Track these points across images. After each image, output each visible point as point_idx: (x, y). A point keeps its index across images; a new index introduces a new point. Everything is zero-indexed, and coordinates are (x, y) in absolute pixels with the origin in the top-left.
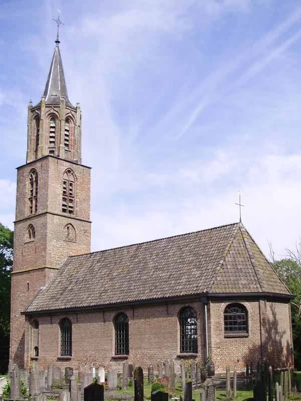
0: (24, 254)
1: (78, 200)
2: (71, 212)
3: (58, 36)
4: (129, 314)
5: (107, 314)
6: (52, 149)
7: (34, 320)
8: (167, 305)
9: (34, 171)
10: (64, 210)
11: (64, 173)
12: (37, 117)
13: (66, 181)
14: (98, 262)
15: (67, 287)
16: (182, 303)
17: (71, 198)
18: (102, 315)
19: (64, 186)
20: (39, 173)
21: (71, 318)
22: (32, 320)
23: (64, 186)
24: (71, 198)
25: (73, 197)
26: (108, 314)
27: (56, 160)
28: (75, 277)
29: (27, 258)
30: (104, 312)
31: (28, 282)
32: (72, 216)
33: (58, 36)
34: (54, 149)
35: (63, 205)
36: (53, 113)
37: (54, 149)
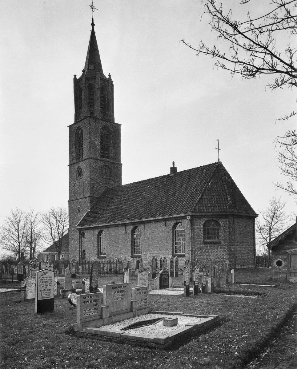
3: (93, 25)
9: (79, 128)
33: (93, 25)
36: (91, 84)
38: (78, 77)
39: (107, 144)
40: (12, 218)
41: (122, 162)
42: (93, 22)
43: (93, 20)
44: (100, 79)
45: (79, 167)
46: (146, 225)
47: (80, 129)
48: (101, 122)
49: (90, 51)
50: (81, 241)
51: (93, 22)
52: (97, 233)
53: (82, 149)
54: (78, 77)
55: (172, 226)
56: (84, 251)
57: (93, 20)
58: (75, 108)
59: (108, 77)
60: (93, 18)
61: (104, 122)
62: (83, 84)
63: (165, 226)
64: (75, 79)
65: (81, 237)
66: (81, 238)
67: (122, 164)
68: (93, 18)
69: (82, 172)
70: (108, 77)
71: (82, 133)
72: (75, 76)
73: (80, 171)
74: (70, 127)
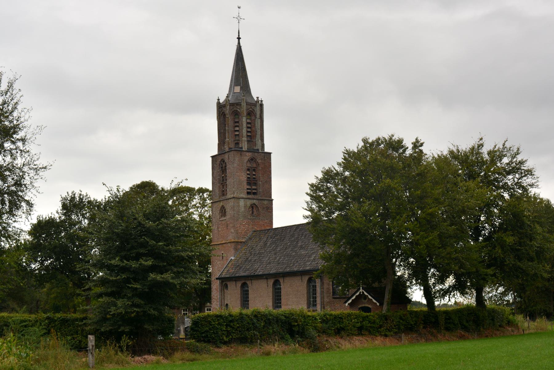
0: (219, 229)
1: (260, 183)
2: (254, 194)
3: (239, 38)
4: (281, 280)
5: (303, 277)
6: (237, 142)
7: (224, 284)
8: (301, 275)
9: (223, 161)
10: (248, 193)
11: (247, 162)
12: (223, 114)
13: (249, 168)
14: (271, 238)
15: (248, 258)
16: (309, 275)
17: (255, 182)
18: (234, 282)
19: (248, 172)
20: (227, 164)
21: (248, 282)
22: (224, 284)
23: (248, 172)
24: (255, 182)
25: (256, 181)
26: (270, 280)
27: (240, 153)
28: (255, 249)
29: (222, 233)
30: (267, 279)
31: (222, 252)
32: (255, 197)
33: (239, 38)
34: (238, 142)
35: (248, 189)
36: (236, 110)
37: (238, 142)
38: (221, 101)
39: (254, 178)
40: (77, 196)
41: (273, 198)
42: (239, 36)
43: (239, 33)
44: (246, 105)
45: (223, 206)
46: (237, 283)
47: (224, 161)
48: (247, 154)
49: (237, 57)
50: (224, 293)
51: (239, 36)
52: (240, 285)
53: (226, 185)
54: (221, 101)
55: (307, 280)
56: (227, 305)
57: (239, 33)
58: (218, 138)
59: (256, 99)
60: (239, 31)
61: (250, 154)
62: (227, 110)
63: (301, 280)
64: (219, 104)
65: (224, 288)
66: (224, 290)
67: (273, 200)
68: (239, 31)
69: (225, 212)
70: (256, 99)
71: (226, 166)
72: (219, 100)
73: (224, 211)
74: (212, 157)
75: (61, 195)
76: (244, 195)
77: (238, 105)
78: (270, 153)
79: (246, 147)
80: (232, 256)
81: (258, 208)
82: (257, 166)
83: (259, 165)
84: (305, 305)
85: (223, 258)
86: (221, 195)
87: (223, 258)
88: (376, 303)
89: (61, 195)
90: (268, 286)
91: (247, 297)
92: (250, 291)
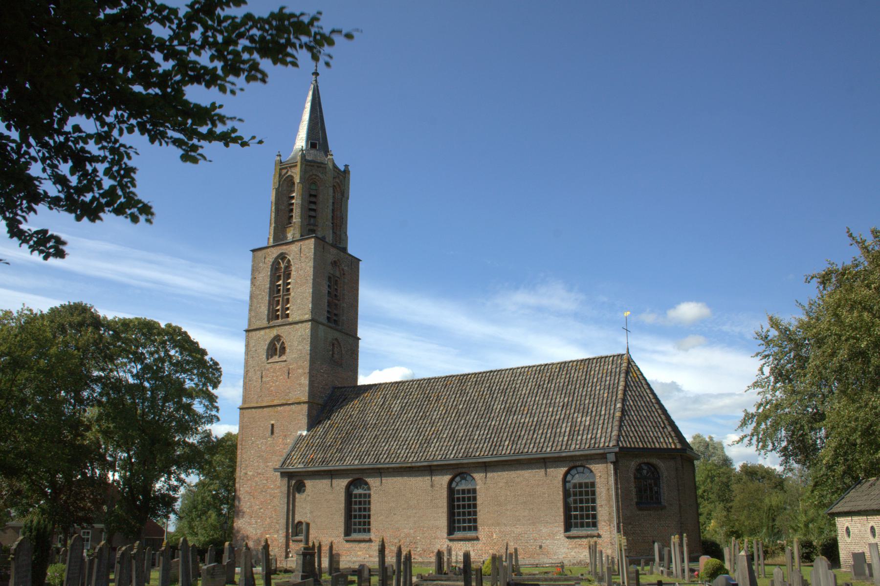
0: (264, 379)
10: (328, 318)
37: (315, 228)
75: (349, 36)
76: (325, 321)
77: (320, 167)
78: (359, 260)
79: (331, 238)
80: (300, 429)
81: (341, 348)
82: (341, 276)
83: (344, 274)
84: (556, 524)
85: (272, 433)
86: (272, 318)
87: (272, 433)
88: (75, 538)
89: (349, 36)
90: (432, 486)
91: (592, 499)
92: (374, 499)
